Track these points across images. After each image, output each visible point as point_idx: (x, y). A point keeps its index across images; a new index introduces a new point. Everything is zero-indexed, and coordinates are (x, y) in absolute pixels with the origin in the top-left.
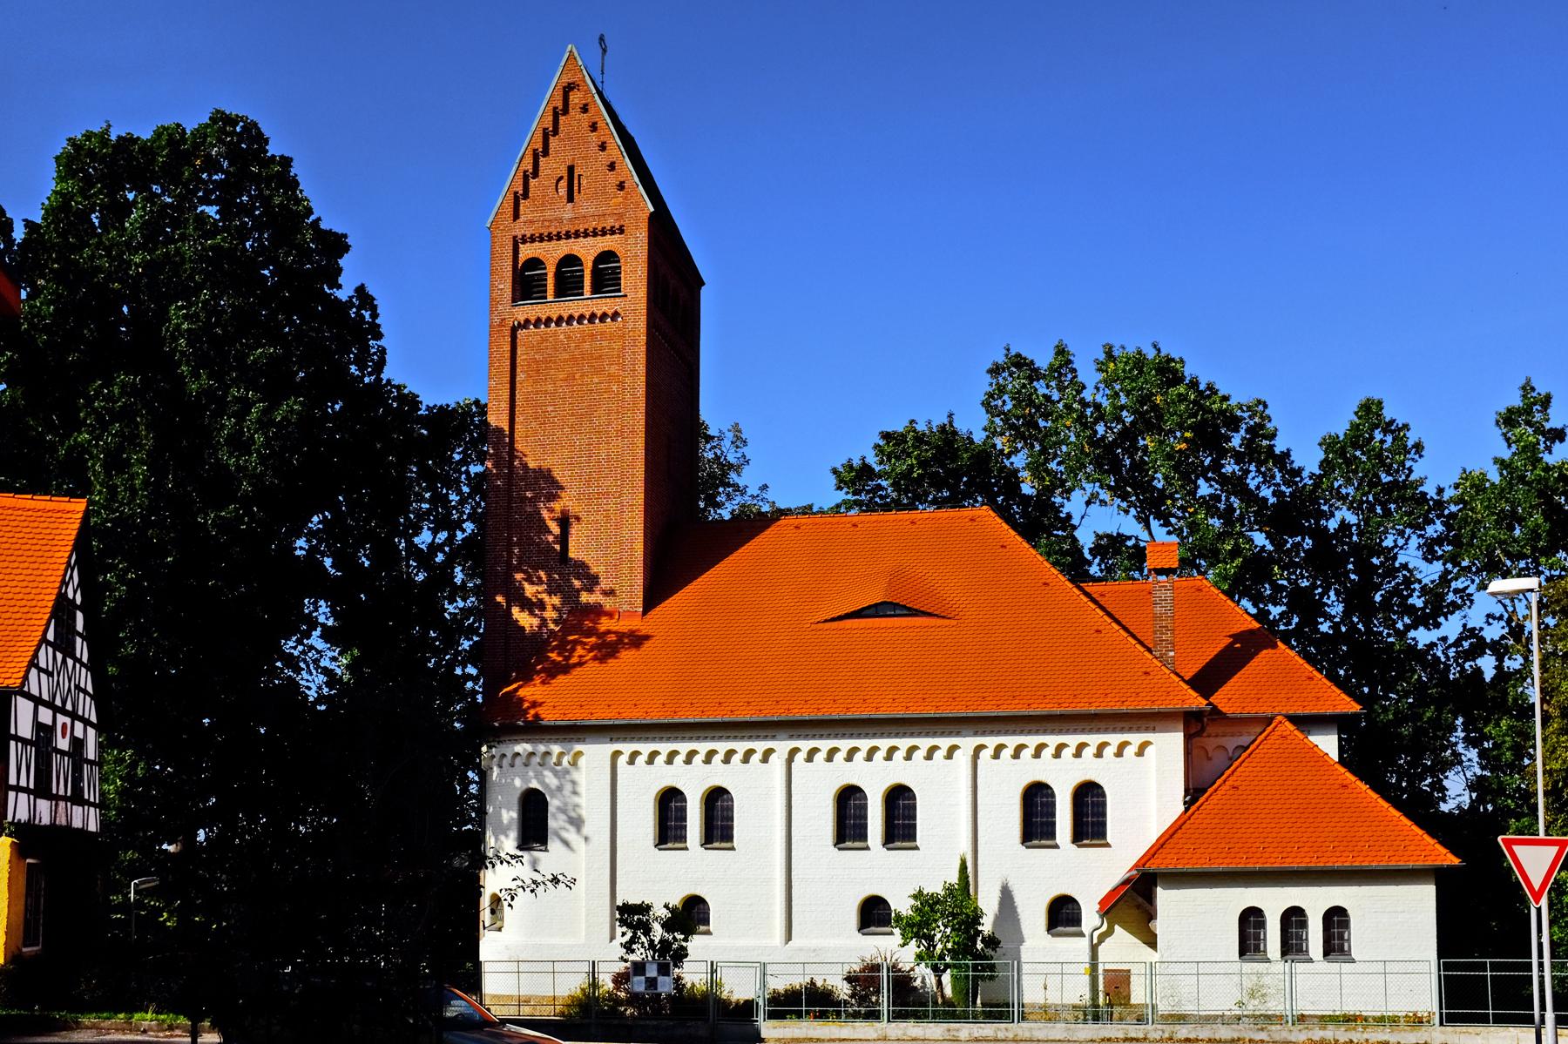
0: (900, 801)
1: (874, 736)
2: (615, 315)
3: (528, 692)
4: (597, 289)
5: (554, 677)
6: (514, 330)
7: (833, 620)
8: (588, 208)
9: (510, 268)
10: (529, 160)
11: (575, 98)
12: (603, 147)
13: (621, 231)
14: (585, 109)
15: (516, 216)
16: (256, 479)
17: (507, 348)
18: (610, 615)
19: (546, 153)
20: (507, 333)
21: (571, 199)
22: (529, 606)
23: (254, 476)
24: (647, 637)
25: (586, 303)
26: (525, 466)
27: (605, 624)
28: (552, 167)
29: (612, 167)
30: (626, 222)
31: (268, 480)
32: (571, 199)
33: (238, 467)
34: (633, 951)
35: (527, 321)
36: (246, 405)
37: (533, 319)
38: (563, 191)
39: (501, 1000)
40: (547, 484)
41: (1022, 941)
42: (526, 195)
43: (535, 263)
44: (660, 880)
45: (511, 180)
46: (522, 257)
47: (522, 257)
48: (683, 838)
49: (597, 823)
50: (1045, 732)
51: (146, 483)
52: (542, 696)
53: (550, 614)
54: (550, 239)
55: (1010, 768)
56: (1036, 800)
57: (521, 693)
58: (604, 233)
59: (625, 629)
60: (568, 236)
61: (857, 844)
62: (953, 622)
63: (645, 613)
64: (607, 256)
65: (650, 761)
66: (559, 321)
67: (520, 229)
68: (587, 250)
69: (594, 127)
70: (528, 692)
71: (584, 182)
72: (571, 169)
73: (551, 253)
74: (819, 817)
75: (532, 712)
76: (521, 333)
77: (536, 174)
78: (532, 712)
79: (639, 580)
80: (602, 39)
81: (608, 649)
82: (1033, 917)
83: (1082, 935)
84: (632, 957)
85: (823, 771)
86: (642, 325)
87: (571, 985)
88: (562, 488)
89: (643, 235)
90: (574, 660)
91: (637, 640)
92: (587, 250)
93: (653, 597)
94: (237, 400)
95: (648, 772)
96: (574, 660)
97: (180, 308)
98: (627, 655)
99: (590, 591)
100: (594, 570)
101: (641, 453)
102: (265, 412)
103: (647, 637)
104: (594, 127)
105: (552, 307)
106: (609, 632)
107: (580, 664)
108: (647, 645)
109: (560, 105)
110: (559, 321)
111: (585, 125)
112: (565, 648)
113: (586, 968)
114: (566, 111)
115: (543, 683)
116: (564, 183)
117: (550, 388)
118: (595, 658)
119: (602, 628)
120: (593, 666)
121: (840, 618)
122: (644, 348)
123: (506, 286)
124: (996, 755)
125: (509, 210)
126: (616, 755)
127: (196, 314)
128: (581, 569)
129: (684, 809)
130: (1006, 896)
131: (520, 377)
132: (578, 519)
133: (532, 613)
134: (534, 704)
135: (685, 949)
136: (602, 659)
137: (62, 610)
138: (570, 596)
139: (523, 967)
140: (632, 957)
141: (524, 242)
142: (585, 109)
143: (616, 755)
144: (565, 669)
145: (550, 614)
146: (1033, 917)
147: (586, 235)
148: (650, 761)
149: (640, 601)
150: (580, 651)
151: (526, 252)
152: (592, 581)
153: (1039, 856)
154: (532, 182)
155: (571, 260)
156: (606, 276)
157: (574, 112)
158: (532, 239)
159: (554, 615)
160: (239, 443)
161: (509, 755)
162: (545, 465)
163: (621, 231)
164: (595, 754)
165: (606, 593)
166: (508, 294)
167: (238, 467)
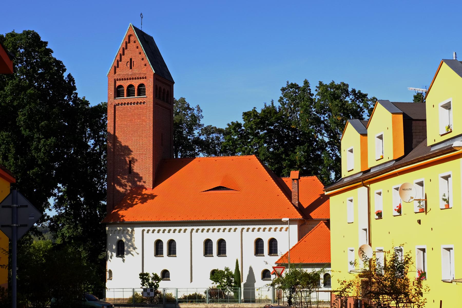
0: (222, 243)
1: (214, 225)
2: (144, 103)
3: (121, 213)
4: (139, 94)
5: (128, 208)
6: (115, 106)
7: (206, 191)
8: (135, 70)
9: (113, 88)
10: (119, 56)
11: (132, 38)
12: (140, 53)
13: (146, 78)
14: (135, 42)
15: (115, 73)
16: (42, 159)
17: (113, 111)
18: (146, 189)
19: (124, 54)
20: (113, 107)
21: (131, 68)
22: (121, 185)
23: (41, 159)
24: (156, 196)
25: (135, 98)
26: (121, 145)
27: (144, 192)
28: (126, 58)
29: (143, 59)
30: (147, 76)
31: (45, 160)
32: (131, 68)
33: (38, 156)
34: (144, 286)
35: (119, 103)
36: (39, 139)
37: (120, 103)
38: (129, 66)
39: (110, 299)
40: (127, 150)
41: (255, 282)
42: (118, 67)
43: (121, 86)
44: (155, 266)
45: (113, 62)
46: (117, 85)
47: (117, 85)
48: (162, 254)
49: (139, 250)
50: (260, 225)
51: (13, 163)
52: (127, 214)
53: (128, 188)
54: (125, 80)
55: (251, 235)
56: (259, 243)
57: (119, 212)
58: (141, 78)
59: (149, 193)
60: (130, 79)
61: (210, 255)
62: (239, 192)
63: (153, 188)
64: (142, 85)
65: (253, 231)
66: (128, 104)
67: (116, 77)
68: (136, 83)
69: (137, 47)
70: (121, 213)
71: (135, 63)
72: (131, 59)
73: (125, 84)
74: (199, 248)
75: (122, 219)
76: (117, 107)
77: (121, 60)
78: (122, 219)
79: (152, 179)
80: (141, 14)
81: (144, 199)
82: (258, 275)
83: (271, 280)
84: (144, 287)
85: (200, 235)
86: (152, 106)
87: (128, 295)
88: (132, 152)
89: (151, 80)
90: (134, 203)
91: (152, 197)
92: (136, 83)
93: (155, 183)
94: (37, 138)
95: (152, 235)
96: (134, 203)
97: (21, 112)
98: (149, 201)
99: (140, 182)
100: (141, 175)
101: (152, 142)
102: (45, 142)
103: (156, 196)
104: (137, 47)
105: (125, 99)
106: (145, 194)
107: (136, 204)
108: (156, 198)
109: (127, 41)
110: (128, 104)
111: (135, 47)
112: (132, 199)
113: (131, 290)
114: (129, 42)
115: (125, 210)
116: (129, 63)
117: (125, 123)
118: (140, 202)
119: (143, 193)
120: (140, 204)
121: (208, 191)
122: (152, 112)
123: (112, 93)
124: (248, 231)
125: (113, 71)
126: (143, 230)
127: (25, 114)
128: (137, 175)
129: (162, 246)
130: (251, 269)
131: (117, 120)
132: (137, 160)
133: (123, 188)
134: (123, 216)
135: (158, 285)
136: (142, 203)
137: (110, 278)
138: (134, 183)
139: (115, 290)
140: (144, 287)
141: (117, 80)
142: (135, 42)
143: (143, 230)
144: (132, 205)
145: (128, 188)
146: (258, 275)
147: (135, 79)
148: (253, 231)
149: (151, 185)
150: (136, 200)
151: (118, 83)
152: (140, 179)
153: (259, 259)
154: (120, 63)
155: (131, 86)
156: (141, 90)
157: (132, 42)
158: (120, 80)
159: (130, 188)
160: (37, 149)
161: (114, 231)
162: (126, 144)
163: (146, 78)
164: (138, 231)
165: (145, 182)
166: (113, 96)
167: (38, 156)
